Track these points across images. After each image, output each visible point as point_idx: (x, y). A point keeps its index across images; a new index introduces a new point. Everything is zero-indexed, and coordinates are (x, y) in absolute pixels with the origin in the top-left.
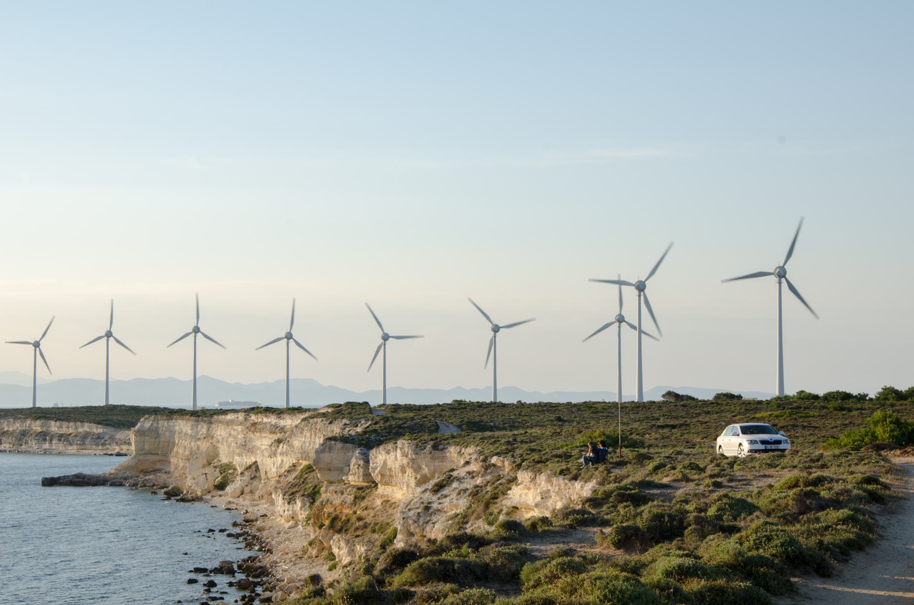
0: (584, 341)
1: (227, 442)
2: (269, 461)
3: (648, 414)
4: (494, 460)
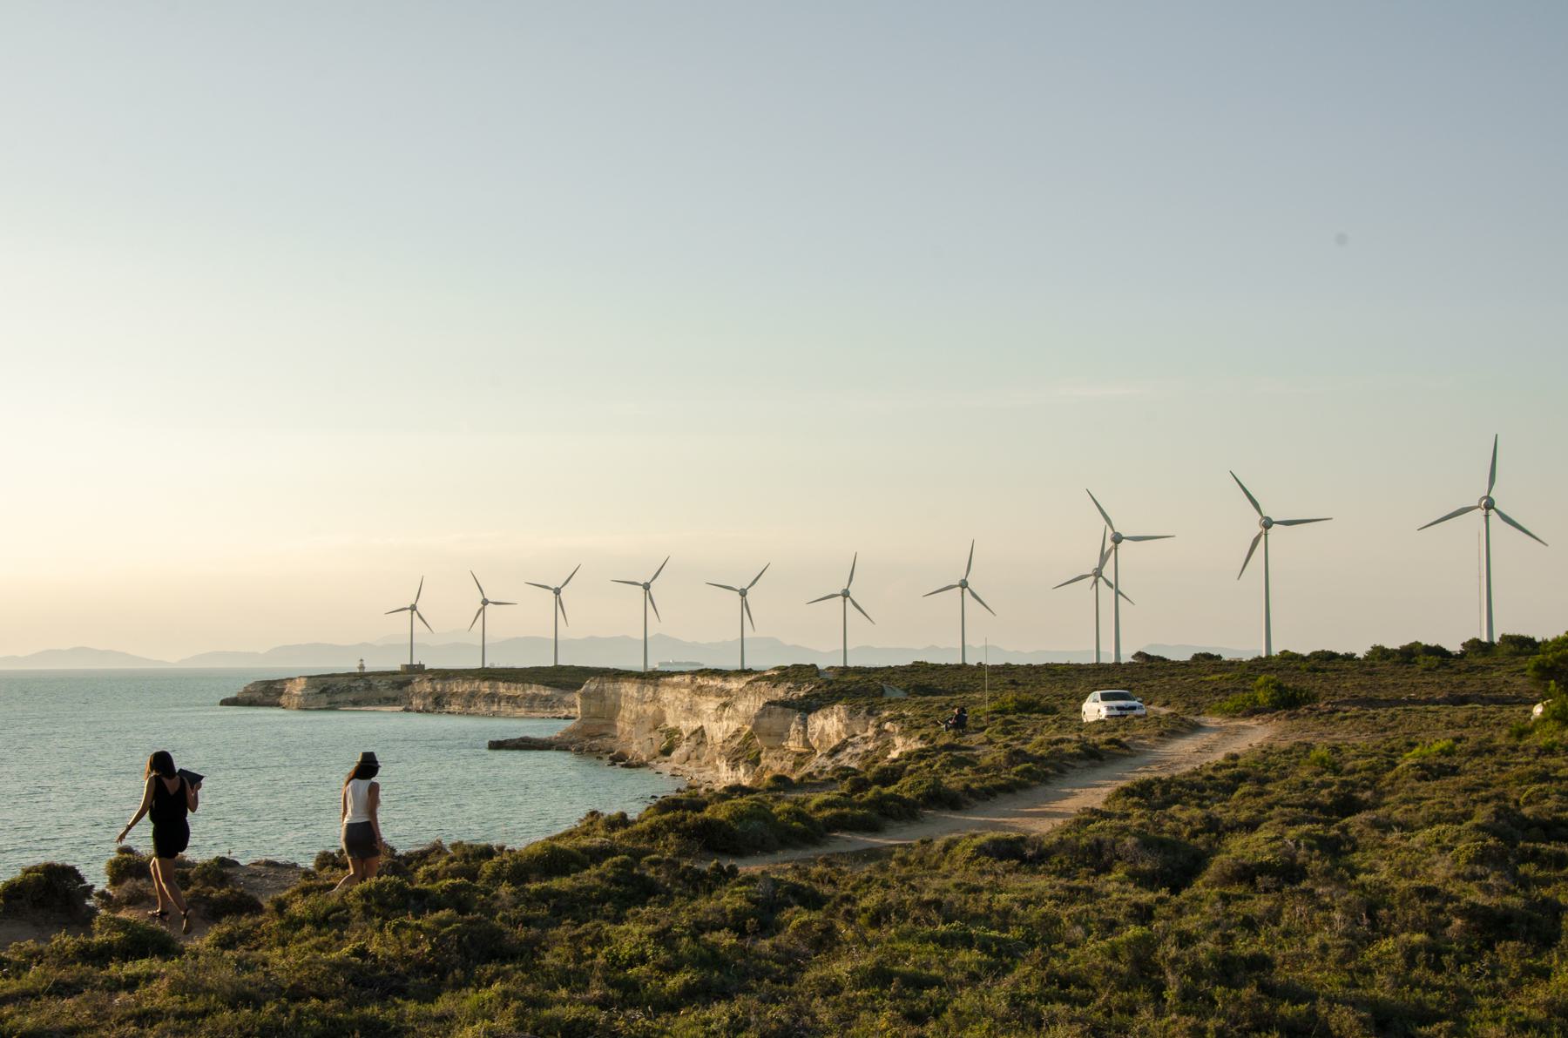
0: (225, 703)
1: (673, 703)
2: (715, 726)
3: (1109, 677)
4: (887, 726)
